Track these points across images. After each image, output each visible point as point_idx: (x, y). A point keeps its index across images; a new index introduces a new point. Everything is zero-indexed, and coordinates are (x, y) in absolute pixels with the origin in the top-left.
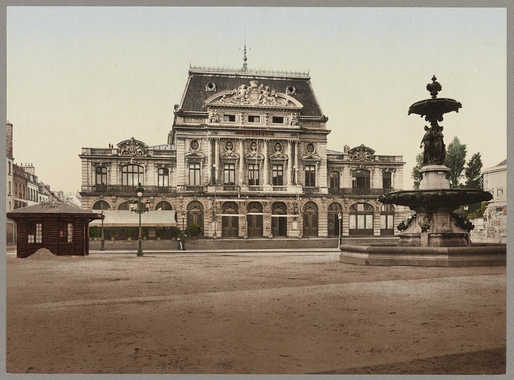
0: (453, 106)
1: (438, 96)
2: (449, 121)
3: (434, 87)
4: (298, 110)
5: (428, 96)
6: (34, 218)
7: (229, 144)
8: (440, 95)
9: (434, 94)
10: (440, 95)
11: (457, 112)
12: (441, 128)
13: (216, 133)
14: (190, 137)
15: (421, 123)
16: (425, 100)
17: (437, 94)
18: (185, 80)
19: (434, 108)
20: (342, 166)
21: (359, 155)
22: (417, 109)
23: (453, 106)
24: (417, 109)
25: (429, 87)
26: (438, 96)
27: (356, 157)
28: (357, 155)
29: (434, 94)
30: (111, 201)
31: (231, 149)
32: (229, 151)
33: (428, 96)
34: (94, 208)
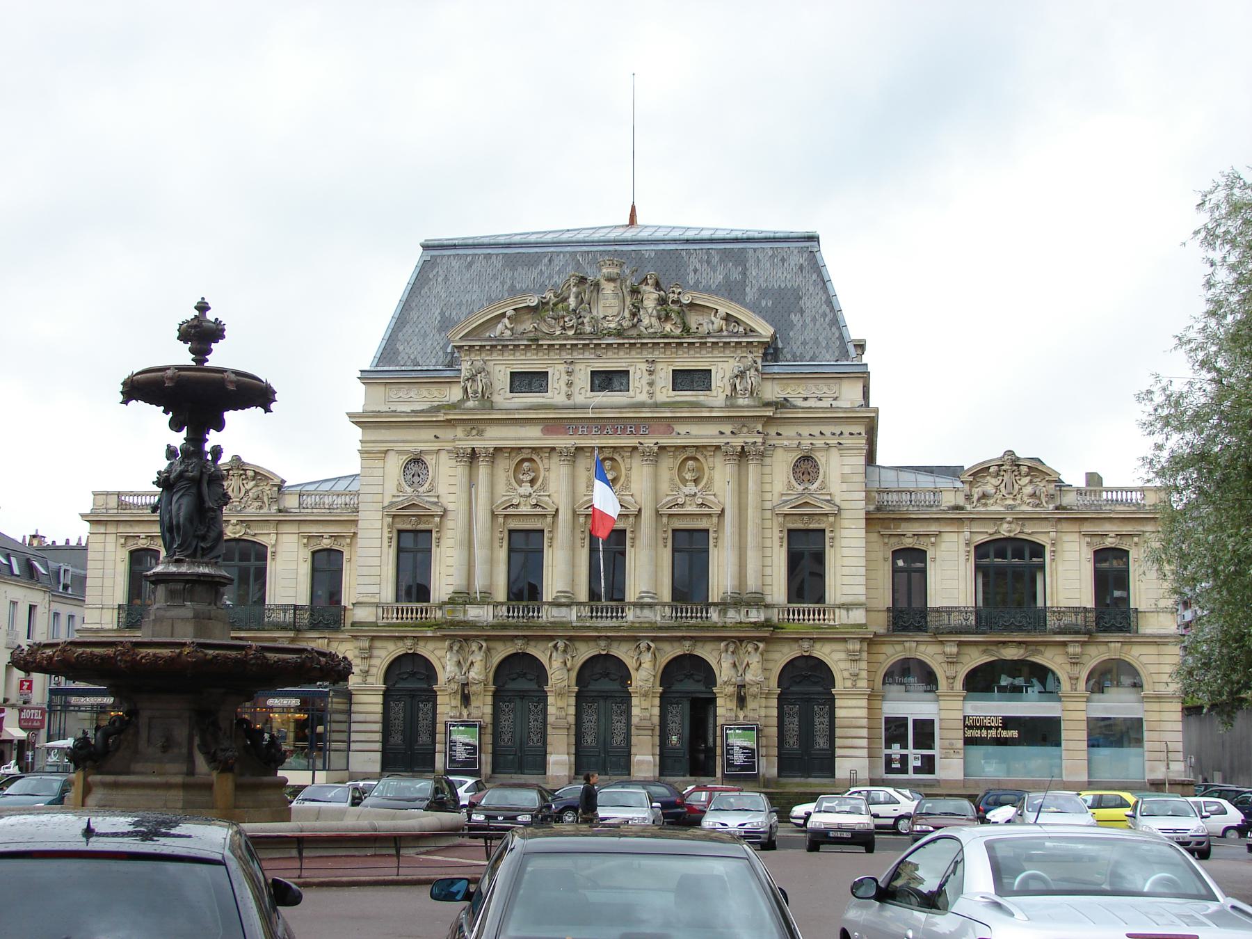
0: (255, 394)
1: (213, 360)
2: (239, 436)
3: (201, 334)
4: (1218, 371)
5: (182, 356)
6: (980, 728)
7: (526, 464)
8: (221, 357)
9: (201, 352)
10: (221, 357)
11: (267, 410)
12: (237, 459)
13: (480, 433)
14: (400, 447)
15: (152, 436)
16: (168, 368)
17: (209, 351)
18: (415, 256)
19: (196, 395)
20: (934, 528)
21: (997, 488)
22: (140, 388)
23: (255, 394)
24: (140, 388)
25: (184, 336)
26: (213, 360)
27: (985, 496)
28: (990, 489)
29: (201, 352)
30: (941, 658)
31: (696, 481)
32: (691, 488)
33: (182, 356)
34: (372, 788)
